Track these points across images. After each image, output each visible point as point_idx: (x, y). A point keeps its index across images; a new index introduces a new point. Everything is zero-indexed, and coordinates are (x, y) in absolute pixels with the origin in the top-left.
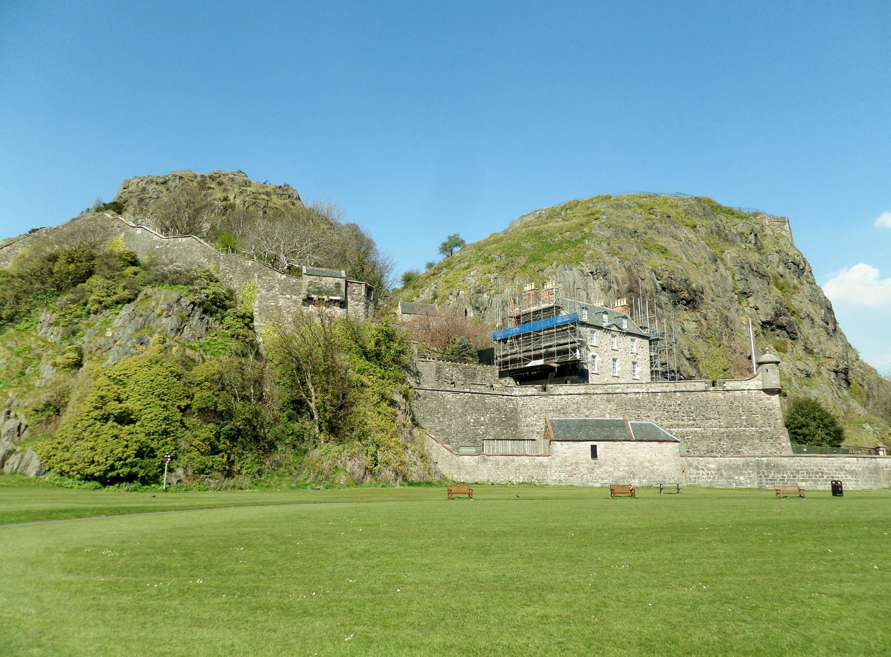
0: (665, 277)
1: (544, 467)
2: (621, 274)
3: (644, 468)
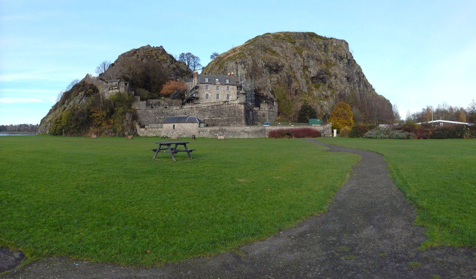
0: (267, 62)
1: (160, 131)
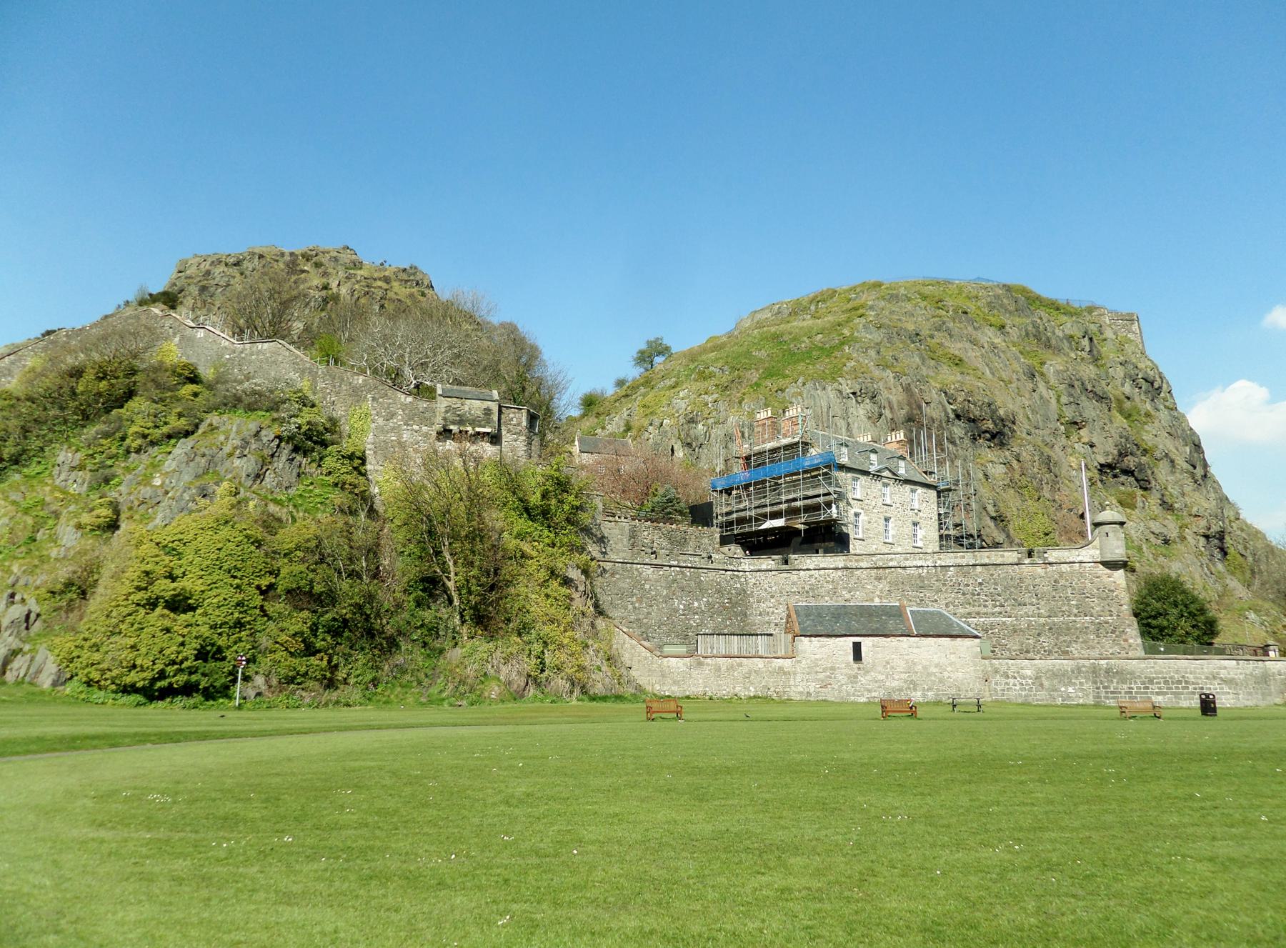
0: (960, 399)
1: (785, 673)
2: (897, 396)
3: (929, 675)
